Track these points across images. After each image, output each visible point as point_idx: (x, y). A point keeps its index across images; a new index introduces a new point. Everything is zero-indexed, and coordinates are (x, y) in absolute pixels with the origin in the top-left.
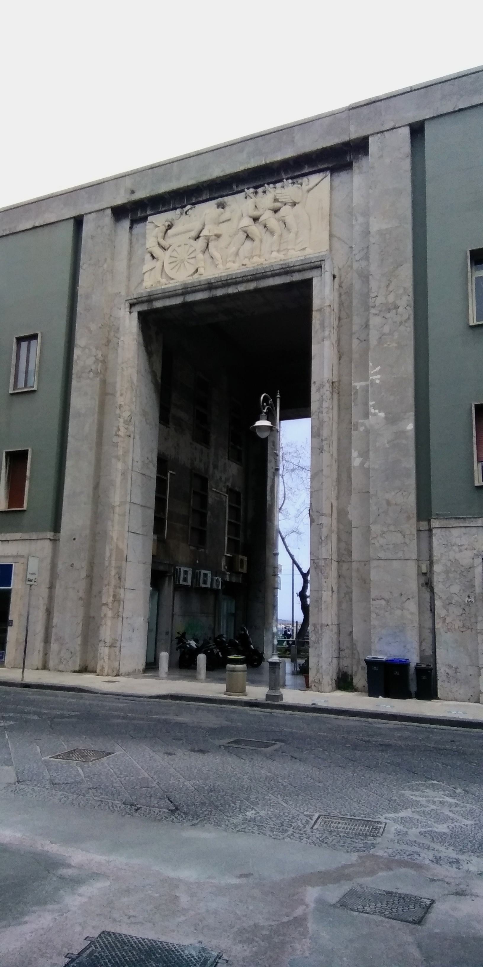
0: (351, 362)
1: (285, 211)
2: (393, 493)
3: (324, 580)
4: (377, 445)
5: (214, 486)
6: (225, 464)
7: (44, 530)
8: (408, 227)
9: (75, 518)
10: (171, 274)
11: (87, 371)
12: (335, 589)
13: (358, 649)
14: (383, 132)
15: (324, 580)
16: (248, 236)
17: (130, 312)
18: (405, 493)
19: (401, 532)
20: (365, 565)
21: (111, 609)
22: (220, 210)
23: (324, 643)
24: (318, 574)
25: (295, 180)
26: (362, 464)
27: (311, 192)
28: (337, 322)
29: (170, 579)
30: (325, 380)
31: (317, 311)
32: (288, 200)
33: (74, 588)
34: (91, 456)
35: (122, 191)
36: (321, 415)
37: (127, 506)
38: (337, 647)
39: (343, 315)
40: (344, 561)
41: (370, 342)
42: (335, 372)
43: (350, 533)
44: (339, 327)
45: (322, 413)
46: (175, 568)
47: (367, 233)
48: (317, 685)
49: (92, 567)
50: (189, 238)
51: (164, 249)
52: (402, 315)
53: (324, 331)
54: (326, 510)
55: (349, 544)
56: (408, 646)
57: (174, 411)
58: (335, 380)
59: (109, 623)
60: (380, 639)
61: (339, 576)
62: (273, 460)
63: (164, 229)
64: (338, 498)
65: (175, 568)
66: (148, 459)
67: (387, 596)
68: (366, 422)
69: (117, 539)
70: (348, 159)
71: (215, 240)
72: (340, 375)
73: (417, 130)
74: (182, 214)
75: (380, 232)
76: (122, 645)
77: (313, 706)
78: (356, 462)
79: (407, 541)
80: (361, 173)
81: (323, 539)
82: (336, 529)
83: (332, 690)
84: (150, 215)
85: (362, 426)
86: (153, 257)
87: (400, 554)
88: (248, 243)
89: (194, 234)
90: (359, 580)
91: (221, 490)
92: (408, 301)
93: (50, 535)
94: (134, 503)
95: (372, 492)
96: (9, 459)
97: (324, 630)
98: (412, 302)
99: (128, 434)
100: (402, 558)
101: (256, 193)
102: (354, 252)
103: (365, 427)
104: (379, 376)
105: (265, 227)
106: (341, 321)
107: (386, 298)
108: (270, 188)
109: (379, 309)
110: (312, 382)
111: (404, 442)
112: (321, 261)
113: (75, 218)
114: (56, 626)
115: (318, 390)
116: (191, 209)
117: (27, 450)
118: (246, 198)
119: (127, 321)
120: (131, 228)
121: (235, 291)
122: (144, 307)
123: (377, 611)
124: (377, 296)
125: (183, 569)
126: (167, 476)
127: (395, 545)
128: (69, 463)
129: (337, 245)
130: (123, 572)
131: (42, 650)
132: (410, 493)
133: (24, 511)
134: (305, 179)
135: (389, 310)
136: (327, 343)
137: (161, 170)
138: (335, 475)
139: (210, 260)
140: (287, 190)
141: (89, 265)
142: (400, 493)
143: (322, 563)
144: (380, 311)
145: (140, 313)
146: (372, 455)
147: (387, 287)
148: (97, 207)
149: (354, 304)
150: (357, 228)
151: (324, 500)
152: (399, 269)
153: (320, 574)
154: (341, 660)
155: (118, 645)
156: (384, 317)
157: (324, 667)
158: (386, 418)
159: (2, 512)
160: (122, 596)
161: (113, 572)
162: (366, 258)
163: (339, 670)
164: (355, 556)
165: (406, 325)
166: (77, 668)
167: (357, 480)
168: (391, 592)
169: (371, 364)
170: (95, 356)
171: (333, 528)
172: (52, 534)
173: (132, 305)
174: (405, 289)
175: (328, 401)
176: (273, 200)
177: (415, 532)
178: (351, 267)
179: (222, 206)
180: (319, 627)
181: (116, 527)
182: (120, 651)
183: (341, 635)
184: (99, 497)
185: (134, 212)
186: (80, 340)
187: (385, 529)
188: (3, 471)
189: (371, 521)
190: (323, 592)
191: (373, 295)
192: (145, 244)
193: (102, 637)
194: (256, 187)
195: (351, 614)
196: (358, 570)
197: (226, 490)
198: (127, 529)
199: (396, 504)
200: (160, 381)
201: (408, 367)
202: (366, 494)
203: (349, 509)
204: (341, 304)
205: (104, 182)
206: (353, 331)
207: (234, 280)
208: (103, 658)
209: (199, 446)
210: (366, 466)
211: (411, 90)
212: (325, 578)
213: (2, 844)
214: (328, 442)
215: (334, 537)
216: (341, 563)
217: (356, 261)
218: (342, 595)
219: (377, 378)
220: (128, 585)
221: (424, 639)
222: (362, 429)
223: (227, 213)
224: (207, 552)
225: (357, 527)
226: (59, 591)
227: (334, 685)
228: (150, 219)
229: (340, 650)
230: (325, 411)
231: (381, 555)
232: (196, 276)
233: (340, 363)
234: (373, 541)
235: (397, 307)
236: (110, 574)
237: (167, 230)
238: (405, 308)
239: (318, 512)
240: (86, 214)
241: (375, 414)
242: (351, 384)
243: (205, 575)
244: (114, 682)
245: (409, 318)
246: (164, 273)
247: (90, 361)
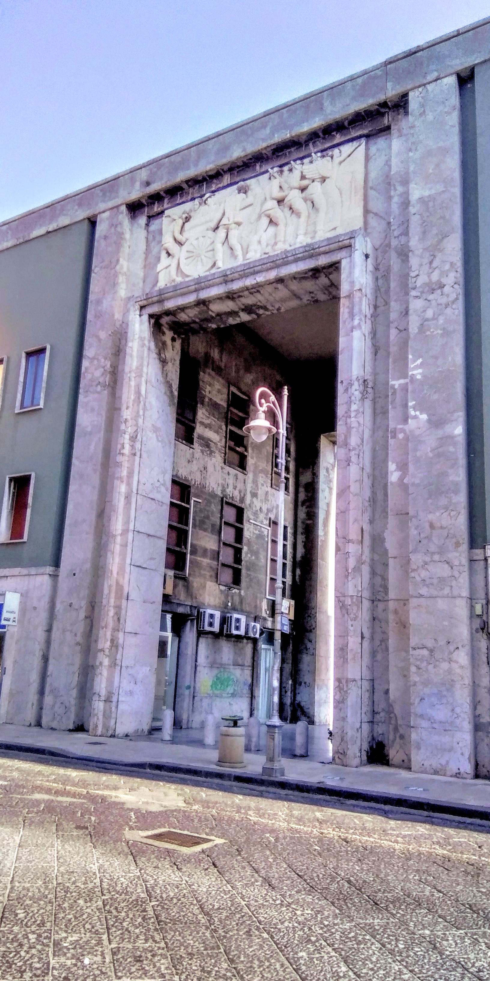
1: (316, 189)
2: (438, 514)
3: (350, 623)
4: (418, 454)
5: (252, 517)
6: (267, 493)
7: (44, 565)
8: (457, 191)
11: (94, 384)
12: (367, 634)
13: (396, 712)
15: (350, 623)
16: (271, 221)
17: (140, 315)
18: (453, 513)
19: (448, 563)
21: (107, 656)
22: (242, 195)
23: (349, 703)
24: (344, 615)
25: (325, 153)
26: (401, 479)
27: (342, 164)
28: (372, 310)
30: (354, 378)
31: (345, 297)
32: (316, 176)
33: (71, 631)
34: (96, 480)
35: (138, 185)
36: (348, 420)
37: (130, 535)
38: (369, 709)
39: (380, 302)
40: (379, 600)
42: (368, 369)
43: (386, 565)
45: (350, 417)
46: (198, 612)
47: (406, 204)
48: (341, 756)
49: (93, 607)
50: (207, 230)
51: (180, 244)
52: (448, 296)
53: (352, 320)
54: (354, 534)
55: (385, 579)
56: (458, 710)
57: (199, 430)
59: (105, 673)
60: (422, 699)
61: (374, 619)
62: (327, 490)
63: (180, 222)
64: (371, 522)
65: (198, 612)
66: (158, 481)
67: (430, 644)
68: (406, 427)
69: (118, 573)
70: (386, 122)
71: (235, 228)
73: (465, 80)
74: (200, 204)
75: (421, 200)
76: (120, 699)
77: (319, 785)
78: (394, 477)
79: (456, 574)
81: (350, 571)
82: (368, 560)
83: (362, 764)
84: (167, 209)
85: (401, 432)
86: (169, 254)
87: (447, 591)
88: (272, 229)
89: (213, 225)
90: (397, 624)
91: (262, 522)
92: (455, 277)
93: (49, 569)
94: (138, 532)
95: (411, 513)
97: (350, 686)
98: (461, 280)
99: (134, 452)
100: (450, 595)
101: (282, 172)
102: (392, 228)
103: (405, 434)
104: (420, 371)
105: (291, 208)
106: (378, 310)
107: (429, 277)
108: (297, 166)
109: (421, 290)
110: (339, 381)
111: (451, 449)
112: (351, 238)
113: (89, 219)
114: (51, 675)
115: (346, 390)
116: (210, 197)
117: (30, 475)
118: (270, 179)
119: (137, 325)
120: (147, 225)
121: (254, 282)
123: (418, 663)
124: (418, 275)
125: (209, 611)
126: (188, 502)
127: (442, 580)
128: (72, 488)
129: (373, 222)
130: (123, 612)
131: (35, 703)
132: (459, 513)
134: (336, 151)
135: (433, 291)
136: (357, 334)
137: (176, 159)
138: (367, 493)
139: (229, 251)
140: (316, 165)
141: (101, 267)
142: (447, 513)
143: (348, 601)
144: (422, 292)
145: (151, 316)
146: (411, 468)
147: (431, 263)
148: (111, 204)
149: (392, 288)
150: (396, 199)
151: (351, 523)
152: (446, 240)
153: (346, 615)
154: (376, 726)
155: (114, 699)
156: (426, 299)
157: (350, 734)
158: (429, 421)
159: (3, 544)
160: (121, 641)
161: (112, 613)
162: (406, 233)
163: (373, 739)
164: (392, 594)
165: (454, 306)
166: (71, 727)
167: (394, 498)
168: (435, 640)
169: (410, 357)
170: (104, 367)
171: (364, 557)
172: (52, 569)
173: (142, 308)
174: (452, 264)
175: (357, 402)
177: (465, 561)
178: (389, 245)
179: (244, 190)
180: (344, 681)
181: (117, 560)
182: (117, 707)
183: (376, 694)
184: (103, 526)
185: (147, 206)
186: (89, 351)
187: (427, 559)
190: (349, 638)
191: (413, 274)
192: (161, 242)
193: (97, 688)
196: (396, 612)
197: (268, 522)
198: (128, 561)
199: (442, 528)
200: (176, 393)
202: (404, 515)
203: (385, 535)
205: (119, 177)
207: (252, 270)
208: (97, 715)
209: (233, 471)
211: (458, 34)
212: (351, 620)
213: (488, 832)
214: (357, 453)
215: (366, 569)
216: (375, 603)
217: (395, 237)
218: (377, 643)
219: (417, 373)
220: (129, 628)
221: (479, 702)
222: (401, 436)
223: (250, 198)
224: (242, 593)
225: (395, 558)
226: (55, 634)
227: (365, 758)
228: (167, 212)
229: (374, 713)
230: (353, 414)
231: (424, 591)
233: (375, 360)
236: (108, 615)
237: (184, 224)
238: (452, 287)
240: (100, 213)
241: (415, 417)
242: (388, 383)
243: (238, 620)
244: (100, 744)
245: (457, 299)
246: (179, 271)
247: (98, 373)
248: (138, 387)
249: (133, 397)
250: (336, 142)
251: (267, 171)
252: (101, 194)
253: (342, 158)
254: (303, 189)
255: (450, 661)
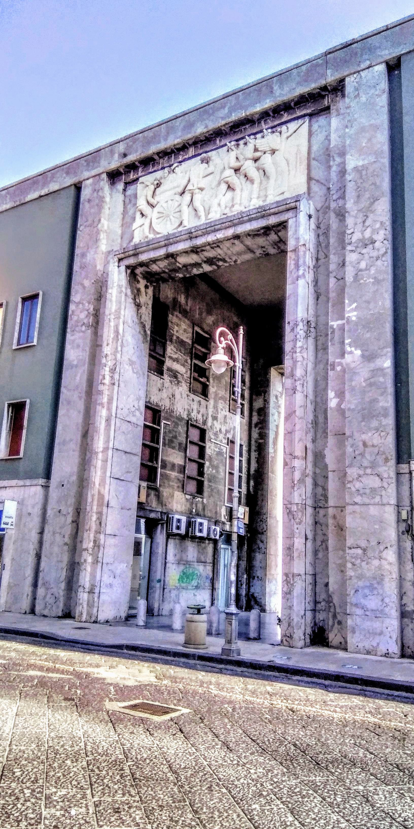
0: (328, 301)
2: (370, 434)
3: (296, 526)
4: (353, 383)
6: (225, 417)
8: (386, 161)
9: (65, 464)
10: (157, 230)
12: (310, 536)
13: (335, 601)
14: (359, 72)
15: (296, 526)
16: (229, 187)
17: (118, 267)
18: (382, 434)
19: (378, 476)
20: (342, 511)
22: (205, 165)
23: (295, 594)
24: (290, 520)
25: (274, 129)
26: (339, 404)
28: (314, 262)
29: (162, 528)
33: (60, 534)
34: (81, 405)
35: (116, 156)
36: (294, 355)
37: (110, 452)
39: (321, 255)
40: (320, 507)
41: (347, 279)
42: (311, 312)
43: (326, 477)
44: (316, 267)
45: (296, 352)
46: (168, 517)
47: (343, 172)
49: (79, 513)
51: (152, 206)
52: (378, 250)
54: (299, 452)
55: (325, 489)
56: (387, 600)
58: (311, 319)
59: (89, 569)
60: (357, 591)
61: (316, 523)
63: (152, 187)
64: (314, 441)
65: (168, 517)
67: (363, 544)
68: (343, 361)
69: (99, 485)
70: (326, 103)
72: (317, 316)
73: (393, 67)
74: (169, 172)
75: (356, 169)
77: (269, 664)
78: (333, 403)
79: (385, 485)
80: (338, 115)
81: (296, 482)
82: (311, 473)
86: (143, 215)
88: (230, 194)
89: (180, 190)
91: (221, 441)
95: (348, 433)
96: (10, 409)
97: (296, 580)
98: (390, 237)
99: (113, 382)
101: (238, 145)
102: (331, 193)
103: (342, 366)
104: (355, 313)
105: (246, 176)
107: (362, 234)
109: (356, 245)
111: (381, 379)
113: (75, 185)
116: (177, 166)
118: (228, 151)
122: (131, 261)
123: (353, 560)
127: (373, 490)
130: (104, 517)
131: (30, 594)
133: (21, 458)
134: (284, 128)
135: (366, 246)
136: (301, 282)
138: (310, 417)
139: (194, 213)
142: (378, 434)
143: (294, 508)
144: (357, 247)
145: (127, 267)
147: (364, 222)
148: (94, 172)
149: (331, 244)
150: (334, 168)
151: (296, 442)
152: (377, 203)
154: (317, 614)
155: (97, 591)
157: (295, 620)
158: (363, 356)
160: (102, 542)
161: (94, 518)
162: (343, 197)
163: (315, 624)
164: (331, 502)
165: (384, 259)
166: (60, 614)
167: (333, 421)
169: (347, 301)
171: (307, 471)
172: (45, 480)
173: (120, 260)
174: (381, 223)
176: (252, 151)
177: (393, 474)
178: (328, 207)
179: (206, 161)
180: (290, 576)
183: (317, 586)
187: (361, 472)
188: (5, 421)
189: (347, 463)
191: (349, 232)
194: (237, 140)
195: (327, 564)
196: (334, 517)
199: (373, 446)
201: (386, 302)
202: (341, 435)
203: (326, 452)
204: (319, 244)
206: (330, 270)
208: (82, 604)
209: (197, 398)
210: (342, 406)
215: (309, 481)
216: (317, 509)
220: (109, 530)
222: (339, 368)
224: (205, 501)
225: (334, 471)
226: (47, 536)
227: (308, 640)
228: (141, 180)
229: (316, 602)
230: (298, 350)
231: (358, 499)
232: (180, 229)
234: (349, 485)
235: (373, 242)
239: (291, 455)
240: (84, 180)
241: (351, 353)
242: (328, 324)
243: (201, 524)
245: (386, 252)
247: (83, 316)
248: (117, 327)
249: (112, 336)
250: (283, 120)
251: (226, 145)
252: (85, 164)
253: (289, 134)
254: (256, 160)
255: (380, 558)
